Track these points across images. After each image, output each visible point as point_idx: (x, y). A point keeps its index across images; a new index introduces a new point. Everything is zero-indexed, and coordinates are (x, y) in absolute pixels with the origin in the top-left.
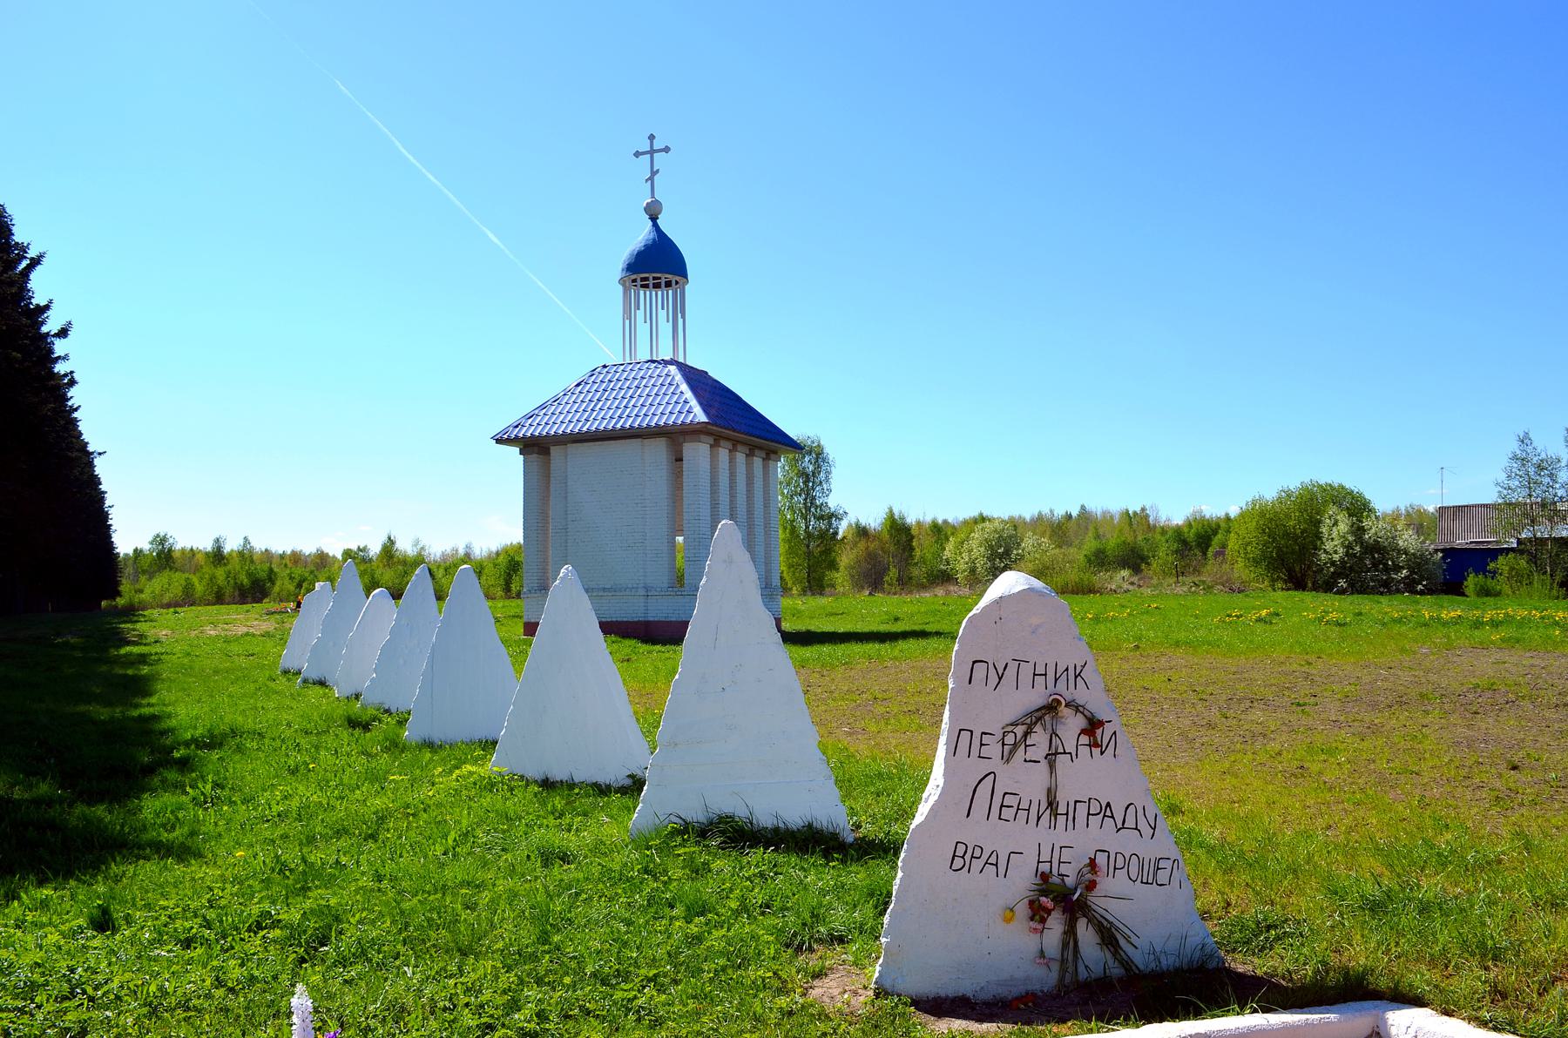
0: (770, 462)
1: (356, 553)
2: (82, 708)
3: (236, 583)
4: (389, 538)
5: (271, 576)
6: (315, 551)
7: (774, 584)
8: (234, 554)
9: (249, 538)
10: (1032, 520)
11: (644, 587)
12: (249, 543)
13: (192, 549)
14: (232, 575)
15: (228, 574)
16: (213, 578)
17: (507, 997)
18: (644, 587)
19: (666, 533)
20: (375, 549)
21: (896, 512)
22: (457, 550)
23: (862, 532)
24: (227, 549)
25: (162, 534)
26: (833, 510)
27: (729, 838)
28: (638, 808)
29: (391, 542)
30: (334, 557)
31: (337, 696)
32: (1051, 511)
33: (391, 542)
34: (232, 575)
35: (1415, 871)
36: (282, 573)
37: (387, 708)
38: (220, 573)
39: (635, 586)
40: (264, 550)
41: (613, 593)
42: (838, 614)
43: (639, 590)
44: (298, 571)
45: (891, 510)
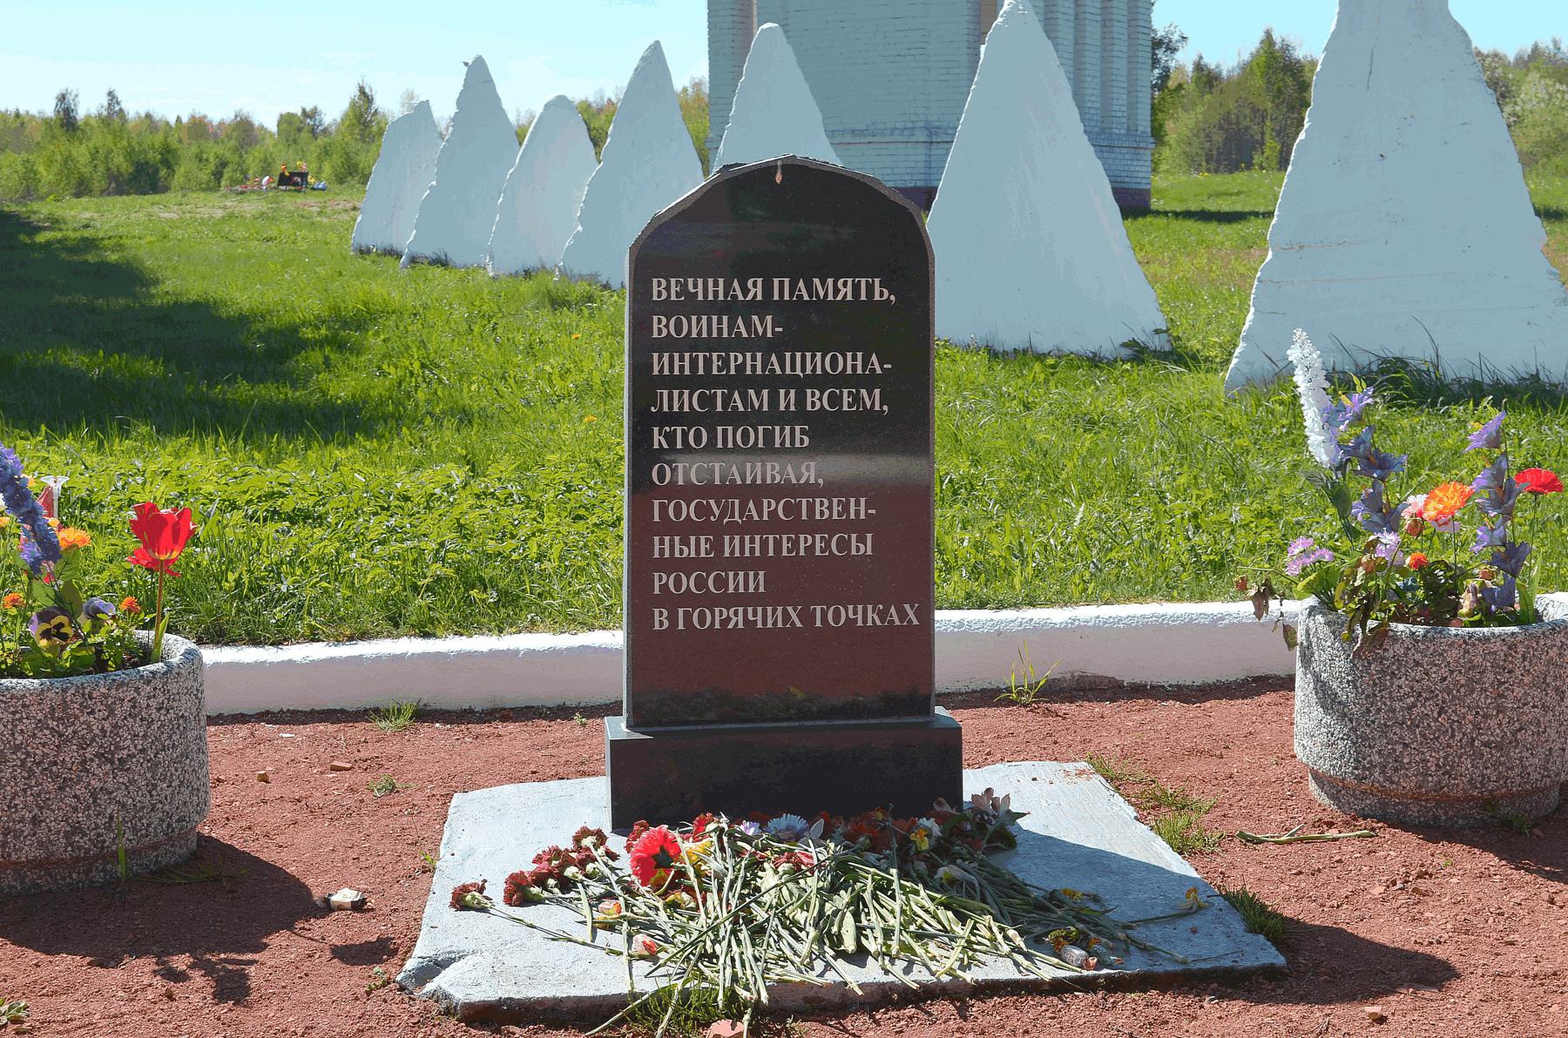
3: (108, 169)
4: (362, 91)
5: (168, 158)
6: (233, 117)
7: (1141, 129)
8: (93, 122)
10: (1519, 59)
11: (926, 128)
12: (118, 103)
13: (18, 115)
14: (101, 156)
15: (94, 155)
16: (68, 159)
18: (926, 128)
19: (966, 31)
20: (333, 111)
21: (1277, 37)
23: (1207, 78)
24: (81, 113)
26: (1160, 33)
27: (1406, 391)
28: (1238, 350)
29: (365, 96)
30: (262, 128)
31: (491, 274)
32: (1555, 43)
33: (365, 96)
34: (101, 156)
36: (188, 151)
37: (604, 283)
38: (81, 152)
39: (909, 125)
40: (143, 115)
41: (871, 139)
42: (1231, 195)
43: (917, 132)
44: (213, 151)
45: (1268, 34)
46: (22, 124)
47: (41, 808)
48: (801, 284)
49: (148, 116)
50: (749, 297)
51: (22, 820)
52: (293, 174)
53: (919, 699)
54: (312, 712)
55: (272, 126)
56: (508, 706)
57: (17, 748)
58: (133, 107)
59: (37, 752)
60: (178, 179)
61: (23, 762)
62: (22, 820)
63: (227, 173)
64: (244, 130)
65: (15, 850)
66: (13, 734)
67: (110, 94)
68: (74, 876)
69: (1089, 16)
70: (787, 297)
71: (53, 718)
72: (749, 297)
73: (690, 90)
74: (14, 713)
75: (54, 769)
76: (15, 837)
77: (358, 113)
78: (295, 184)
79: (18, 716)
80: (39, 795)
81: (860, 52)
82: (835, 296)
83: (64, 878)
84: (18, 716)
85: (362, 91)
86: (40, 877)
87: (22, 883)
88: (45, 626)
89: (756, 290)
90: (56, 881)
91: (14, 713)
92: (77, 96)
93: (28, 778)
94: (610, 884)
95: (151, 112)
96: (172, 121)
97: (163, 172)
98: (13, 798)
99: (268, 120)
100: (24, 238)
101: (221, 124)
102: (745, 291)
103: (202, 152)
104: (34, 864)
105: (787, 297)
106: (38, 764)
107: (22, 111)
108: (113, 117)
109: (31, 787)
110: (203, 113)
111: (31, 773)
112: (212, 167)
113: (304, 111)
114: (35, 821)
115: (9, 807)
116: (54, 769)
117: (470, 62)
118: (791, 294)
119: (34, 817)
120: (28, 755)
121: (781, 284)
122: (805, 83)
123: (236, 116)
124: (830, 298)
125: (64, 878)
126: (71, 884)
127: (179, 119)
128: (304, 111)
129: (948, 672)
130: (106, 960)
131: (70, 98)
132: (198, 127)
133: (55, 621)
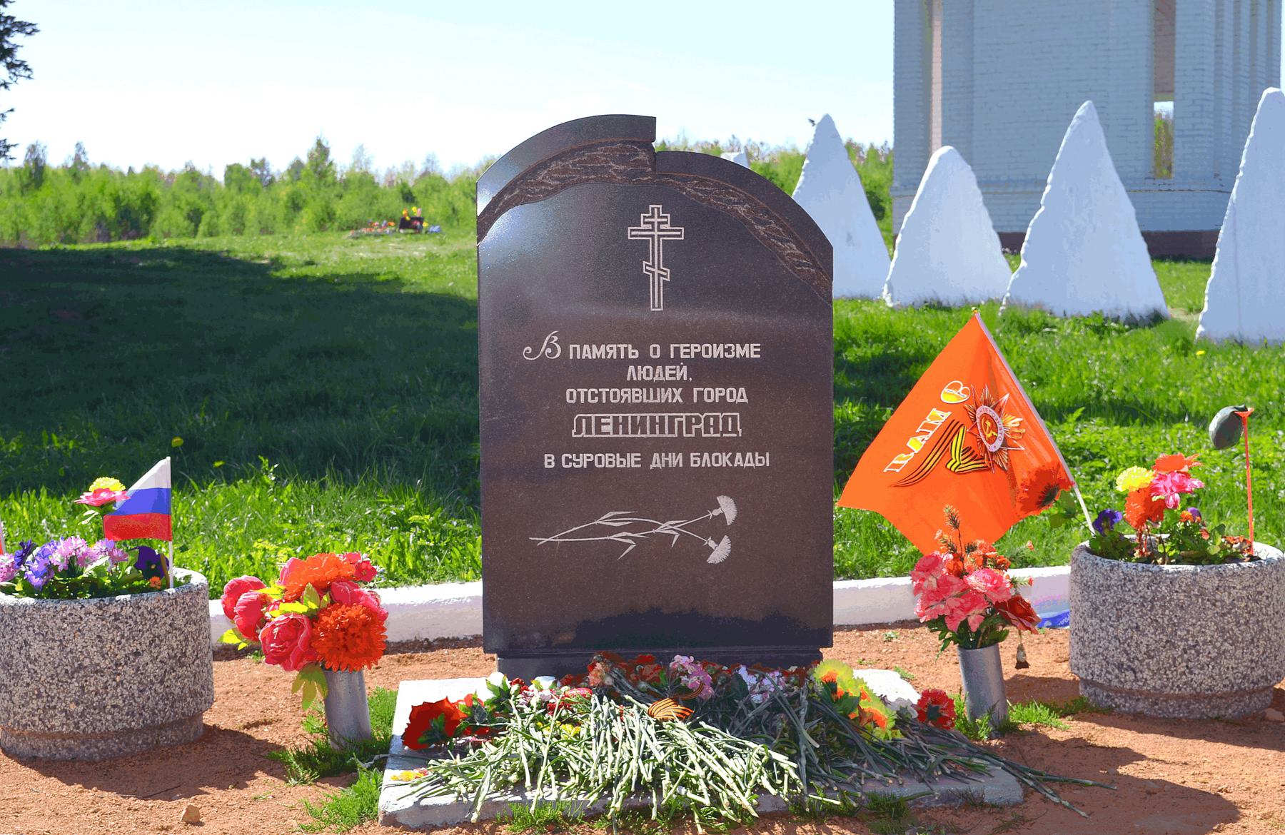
4: (319, 144)
5: (148, 204)
14: (87, 203)
22: (412, 166)
34: (87, 203)
49: (103, 166)
54: (876, 624)
55: (220, 177)
56: (909, 619)
58: (94, 159)
63: (206, 218)
64: (192, 176)
69: (1242, 79)
77: (315, 163)
78: (415, 228)
81: (1043, 111)
85: (319, 144)
92: (45, 147)
94: (556, 728)
96: (126, 171)
101: (171, 175)
108: (78, 171)
110: (155, 163)
113: (253, 162)
123: (186, 166)
128: (253, 162)
130: (70, 784)
131: (40, 148)
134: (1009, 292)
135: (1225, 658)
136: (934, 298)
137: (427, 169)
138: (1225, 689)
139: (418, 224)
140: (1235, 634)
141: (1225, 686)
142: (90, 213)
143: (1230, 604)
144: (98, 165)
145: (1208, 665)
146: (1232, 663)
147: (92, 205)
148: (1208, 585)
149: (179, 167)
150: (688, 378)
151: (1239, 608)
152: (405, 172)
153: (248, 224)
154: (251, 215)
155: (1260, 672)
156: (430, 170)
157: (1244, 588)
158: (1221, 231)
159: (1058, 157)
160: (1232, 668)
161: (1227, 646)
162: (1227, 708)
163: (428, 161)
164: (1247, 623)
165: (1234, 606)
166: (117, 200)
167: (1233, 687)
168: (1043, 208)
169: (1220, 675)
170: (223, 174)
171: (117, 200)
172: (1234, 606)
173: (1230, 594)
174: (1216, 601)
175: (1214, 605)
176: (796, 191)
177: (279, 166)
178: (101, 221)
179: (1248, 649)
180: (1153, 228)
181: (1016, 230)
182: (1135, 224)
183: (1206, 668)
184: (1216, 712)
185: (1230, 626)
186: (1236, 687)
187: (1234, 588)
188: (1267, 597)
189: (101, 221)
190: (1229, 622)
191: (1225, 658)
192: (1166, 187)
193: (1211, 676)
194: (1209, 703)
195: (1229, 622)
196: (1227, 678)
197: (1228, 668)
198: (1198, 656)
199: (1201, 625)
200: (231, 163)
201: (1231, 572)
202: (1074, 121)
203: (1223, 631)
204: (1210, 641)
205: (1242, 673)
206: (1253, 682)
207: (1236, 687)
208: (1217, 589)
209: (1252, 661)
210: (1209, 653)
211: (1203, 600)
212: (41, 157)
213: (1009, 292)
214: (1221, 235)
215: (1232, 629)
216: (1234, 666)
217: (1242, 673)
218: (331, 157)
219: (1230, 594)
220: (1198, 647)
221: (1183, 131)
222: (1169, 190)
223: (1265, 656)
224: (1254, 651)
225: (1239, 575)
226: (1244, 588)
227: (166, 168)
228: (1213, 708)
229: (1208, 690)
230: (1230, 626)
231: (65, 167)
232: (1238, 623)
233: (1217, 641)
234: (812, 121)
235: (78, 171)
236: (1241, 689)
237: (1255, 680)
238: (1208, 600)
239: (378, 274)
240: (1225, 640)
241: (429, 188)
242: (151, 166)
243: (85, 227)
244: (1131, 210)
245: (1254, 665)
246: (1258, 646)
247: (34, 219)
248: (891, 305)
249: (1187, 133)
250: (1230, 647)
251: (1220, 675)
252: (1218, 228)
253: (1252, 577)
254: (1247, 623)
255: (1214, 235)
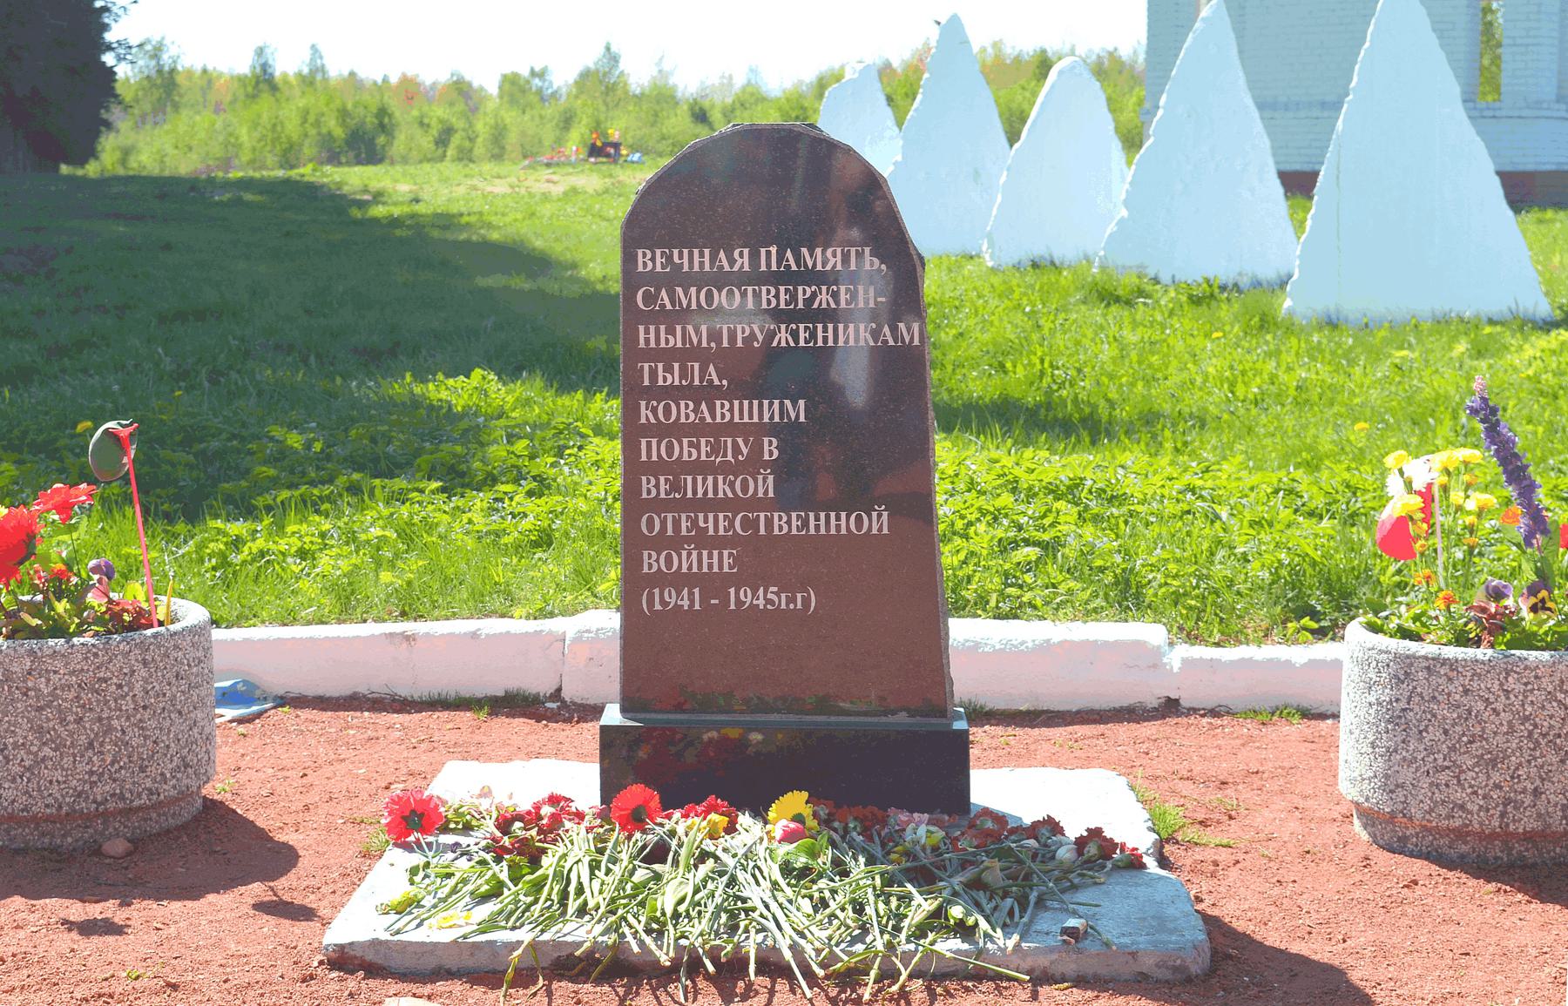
0: (180, 68)
1: (528, 82)
2: (405, 386)
4: (608, 49)
5: (384, 122)
9: (318, 47)
12: (321, 58)
13: (205, 71)
14: (311, 118)
17: (788, 955)
22: (731, 77)
25: (155, 39)
30: (482, 89)
34: (311, 118)
35: (1198, 586)
46: (210, 82)
47: (1543, 780)
48: (722, 255)
49: (352, 74)
50: (736, 268)
51: (1524, 791)
52: (606, 145)
53: (941, 710)
55: (493, 89)
57: (1527, 718)
59: (1545, 724)
60: (399, 145)
61: (1531, 733)
62: (1524, 791)
63: (456, 140)
64: (462, 90)
65: (1514, 821)
66: (1523, 705)
67: (313, 47)
68: (1558, 850)
70: (774, 268)
71: (1561, 691)
72: (736, 268)
73: (990, 50)
74: (1526, 684)
75: (1558, 741)
76: (1515, 808)
78: (608, 155)
79: (1529, 687)
80: (1542, 767)
81: (1334, 11)
82: (824, 265)
83: (1549, 852)
84: (1529, 687)
86: (1527, 850)
87: (1508, 855)
88: (1533, 600)
89: (743, 261)
90: (1541, 854)
91: (1526, 684)
93: (1534, 749)
95: (356, 70)
96: (380, 81)
97: (381, 140)
98: (1517, 769)
99: (487, 81)
100: (356, 213)
102: (732, 262)
103: (422, 117)
104: (1528, 837)
105: (774, 268)
106: (1544, 736)
107: (210, 68)
109: (1535, 759)
111: (1537, 743)
112: (434, 132)
114: (1537, 793)
115: (1512, 777)
116: (1558, 741)
117: (943, 22)
118: (779, 264)
119: (1536, 789)
120: (1536, 726)
121: (769, 253)
122: (1440, 50)
123: (452, 75)
124: (819, 267)
125: (1549, 852)
126: (1554, 858)
127: (385, 80)
129: (966, 682)
131: (268, 51)
132: (410, 89)
133: (1540, 596)
134: (1104, 249)
135: (46, 768)
136: (1047, 256)
137: (749, 82)
138: (48, 811)
139: (612, 151)
140: (59, 736)
141: (47, 806)
142: (313, 132)
143: (50, 694)
144: (198, 67)
145: (21, 777)
146: (58, 775)
147: (317, 124)
148: (15, 668)
149: (443, 77)
150: (708, 344)
151: (65, 700)
152: (722, 84)
153: (509, 148)
154: (512, 138)
155: (107, 788)
156: (753, 82)
157: (72, 673)
158: (1322, 173)
159: (1174, 73)
160: (57, 781)
161: (47, 751)
162: (64, 836)
163: (752, 70)
164: (79, 720)
165: (56, 697)
166: (344, 114)
167: (60, 807)
168: (1152, 140)
169: (39, 790)
170: (497, 85)
171: (344, 114)
172: (56, 697)
173: (48, 680)
174: (29, 689)
175: (25, 694)
176: (911, 113)
177: (563, 77)
178: (326, 142)
179: (82, 756)
180: (1288, 167)
181: (1307, 168)
182: (1270, 162)
183: (19, 780)
184: (46, 840)
185: (51, 724)
186: (65, 809)
187: (55, 672)
188: (120, 686)
189: (326, 142)
190: (48, 720)
191: (46, 768)
192: (1491, 113)
193: (27, 792)
194: (36, 828)
195: (48, 720)
196: (50, 795)
197: (51, 782)
198: (7, 763)
199: (8, 722)
200: (508, 71)
201: (51, 651)
202: (1197, 25)
203: (40, 730)
204: (23, 744)
205: (75, 790)
206: (95, 801)
207: (65, 809)
208: (29, 674)
209: (91, 773)
210: (22, 760)
211: (10, 687)
212: (270, 62)
213: (1104, 249)
214: (1320, 178)
215: (54, 729)
216: (60, 779)
217: (75, 790)
218: (622, 66)
219: (48, 680)
220: (6, 752)
221: (1514, 38)
222: (1494, 117)
223: (117, 766)
224: (95, 758)
225: (63, 655)
226: (72, 673)
227: (427, 78)
228: (43, 834)
229: (23, 810)
230: (51, 724)
231: (299, 75)
232: (63, 721)
233: (32, 744)
234: (939, 23)
235: (312, 80)
236: (75, 811)
237: (99, 798)
238: (17, 688)
239: (461, 215)
240: (44, 744)
241: (738, 105)
242: (409, 74)
243: (308, 150)
244: (1265, 143)
245: (94, 778)
246: (101, 753)
247: (244, 135)
248: (990, 264)
249: (1519, 41)
250: (52, 754)
251: (39, 790)
252: (1317, 167)
253: (86, 658)
254: (79, 720)
255: (1315, 174)
